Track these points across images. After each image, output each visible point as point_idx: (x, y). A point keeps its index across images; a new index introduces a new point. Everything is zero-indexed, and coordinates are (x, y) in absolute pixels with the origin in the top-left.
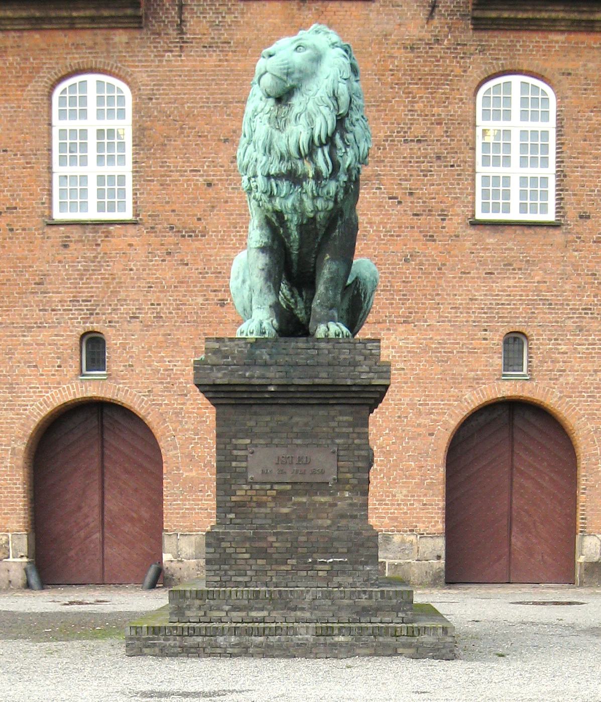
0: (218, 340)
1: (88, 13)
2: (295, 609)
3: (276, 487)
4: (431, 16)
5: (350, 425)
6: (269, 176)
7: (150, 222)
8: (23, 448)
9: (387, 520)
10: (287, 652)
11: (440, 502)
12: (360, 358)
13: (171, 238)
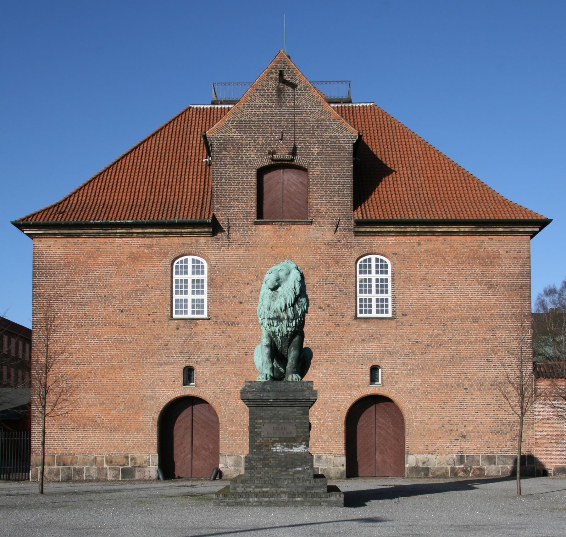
0: (250, 382)
1: (189, 230)
2: (280, 487)
3: (273, 439)
4: (336, 231)
5: (302, 414)
6: (269, 319)
7: (215, 319)
8: (157, 417)
9: (319, 449)
10: (276, 504)
11: (342, 440)
12: (305, 389)
13: (224, 326)
